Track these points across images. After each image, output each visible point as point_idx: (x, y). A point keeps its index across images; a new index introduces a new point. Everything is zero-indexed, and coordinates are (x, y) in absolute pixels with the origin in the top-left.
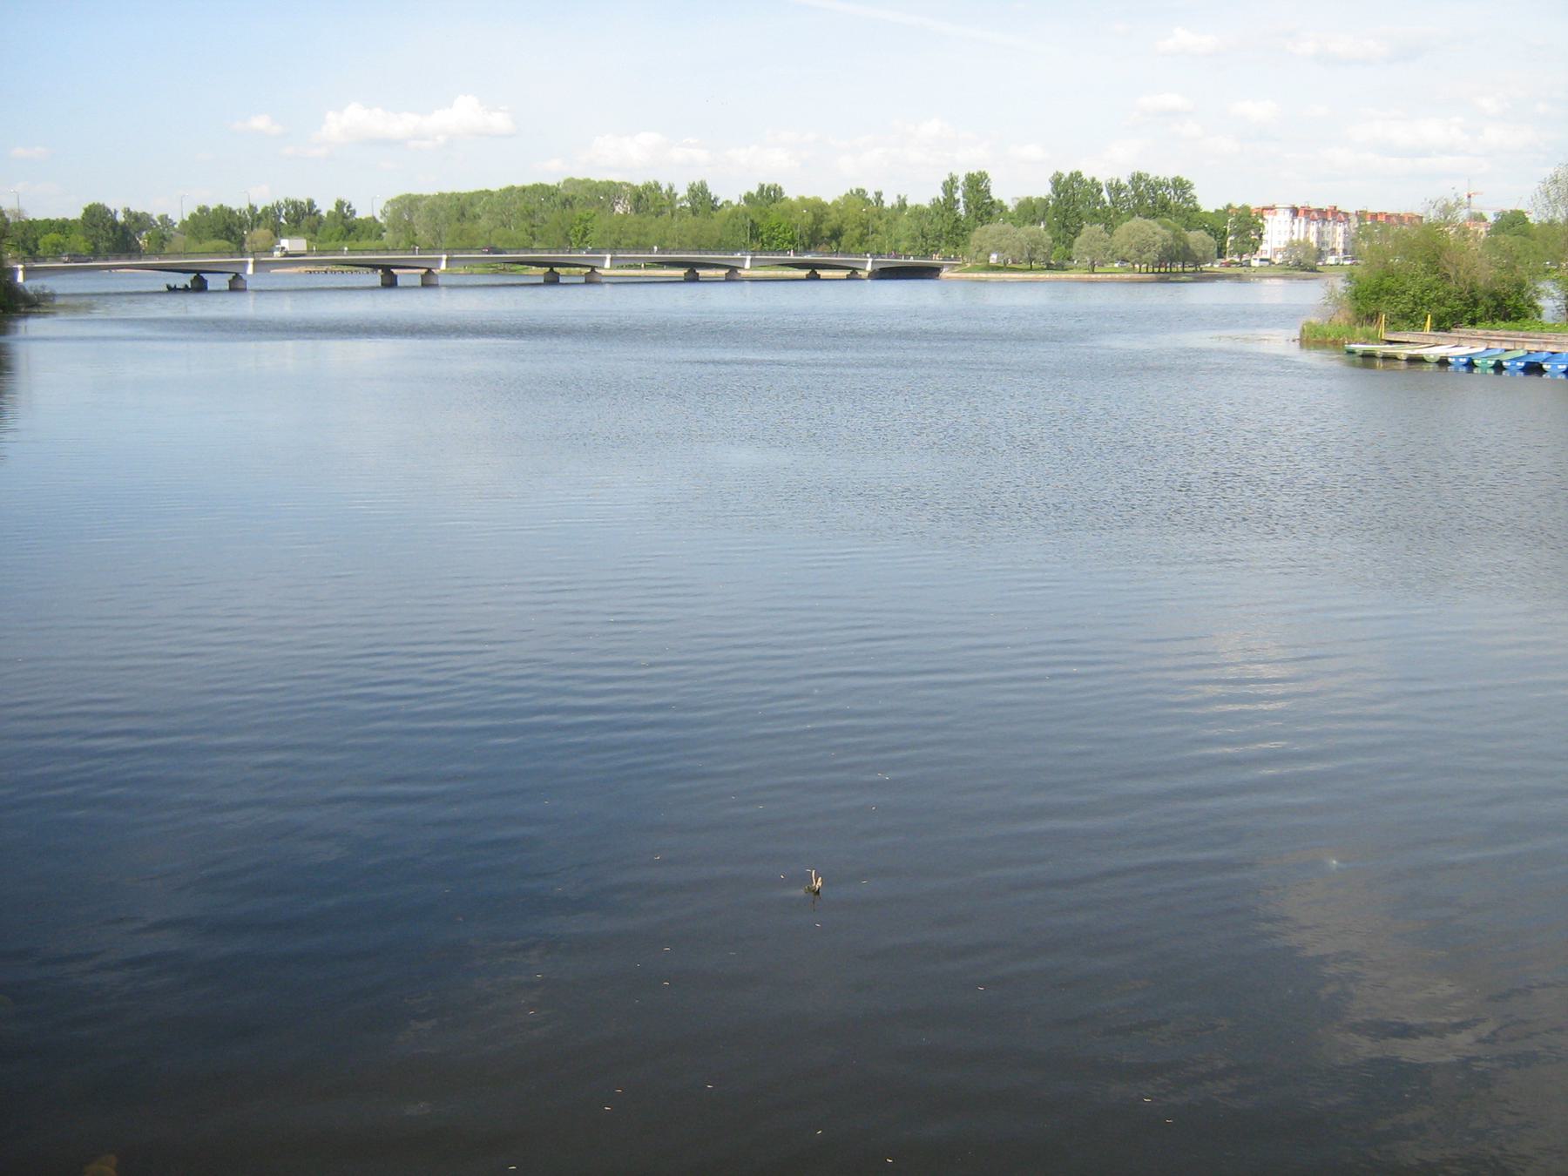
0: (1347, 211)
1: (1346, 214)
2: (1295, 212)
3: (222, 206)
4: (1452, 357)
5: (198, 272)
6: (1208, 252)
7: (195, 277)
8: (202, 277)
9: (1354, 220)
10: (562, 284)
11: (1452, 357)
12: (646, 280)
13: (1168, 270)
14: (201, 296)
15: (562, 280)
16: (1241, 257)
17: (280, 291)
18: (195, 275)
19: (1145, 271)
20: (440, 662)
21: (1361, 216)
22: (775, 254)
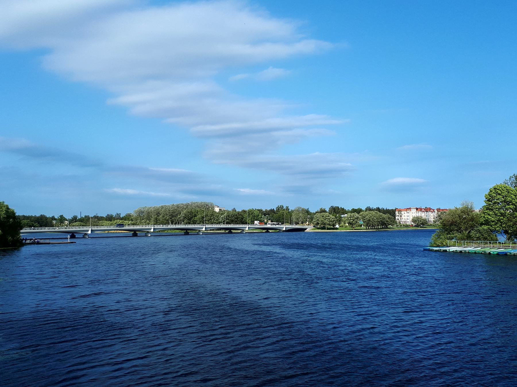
0: (390, 208)
1: (434, 210)
2: (417, 209)
3: (63, 215)
4: (492, 252)
5: (73, 233)
6: (21, 237)
7: (72, 234)
8: (74, 234)
9: (436, 211)
10: (138, 236)
11: (492, 252)
12: (217, 233)
13: (372, 228)
14: (135, 238)
15: (190, 234)
16: (38, 241)
17: (172, 235)
18: (133, 232)
19: (370, 228)
20: (161, 380)
21: (438, 210)
22: (209, 225)
